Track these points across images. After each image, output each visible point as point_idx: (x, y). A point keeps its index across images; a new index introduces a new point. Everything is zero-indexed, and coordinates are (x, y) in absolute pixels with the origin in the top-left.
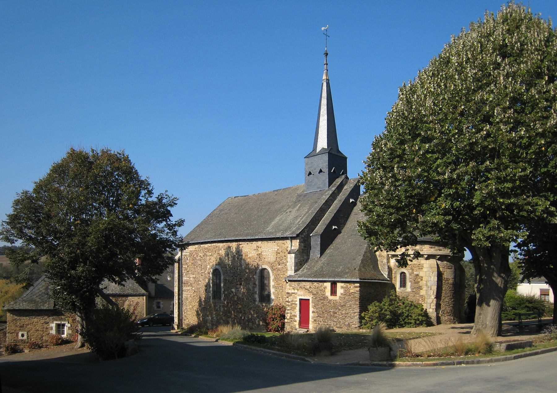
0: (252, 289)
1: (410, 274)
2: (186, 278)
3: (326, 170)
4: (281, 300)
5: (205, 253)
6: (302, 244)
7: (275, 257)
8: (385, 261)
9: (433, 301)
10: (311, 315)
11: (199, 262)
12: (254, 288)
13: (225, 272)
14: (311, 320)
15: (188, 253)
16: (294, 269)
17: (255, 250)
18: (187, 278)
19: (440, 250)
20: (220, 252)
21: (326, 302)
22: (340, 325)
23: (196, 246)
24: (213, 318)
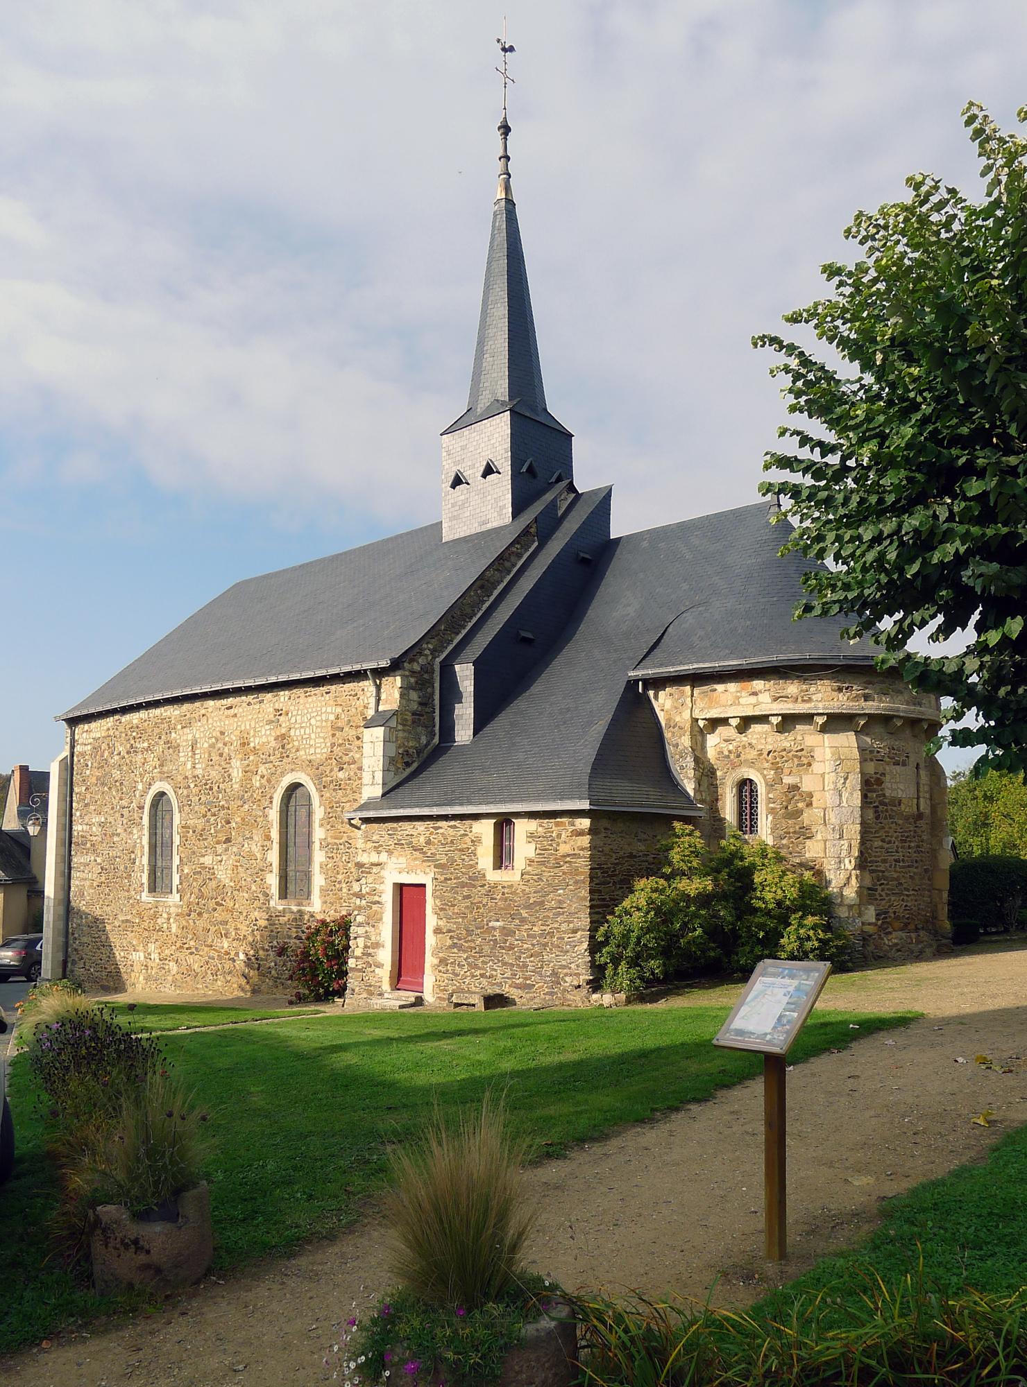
0: (259, 856)
1: (770, 786)
2: (80, 828)
3: (505, 466)
4: (344, 890)
5: (132, 742)
6: (414, 695)
7: (329, 744)
8: (686, 741)
9: (849, 878)
10: (430, 940)
11: (117, 774)
12: (265, 849)
13: (185, 803)
14: (430, 960)
15: (89, 747)
16: (381, 782)
18: (85, 827)
19: (867, 698)
20: (173, 735)
21: (478, 893)
22: (526, 979)
23: (110, 721)
24: (149, 954)
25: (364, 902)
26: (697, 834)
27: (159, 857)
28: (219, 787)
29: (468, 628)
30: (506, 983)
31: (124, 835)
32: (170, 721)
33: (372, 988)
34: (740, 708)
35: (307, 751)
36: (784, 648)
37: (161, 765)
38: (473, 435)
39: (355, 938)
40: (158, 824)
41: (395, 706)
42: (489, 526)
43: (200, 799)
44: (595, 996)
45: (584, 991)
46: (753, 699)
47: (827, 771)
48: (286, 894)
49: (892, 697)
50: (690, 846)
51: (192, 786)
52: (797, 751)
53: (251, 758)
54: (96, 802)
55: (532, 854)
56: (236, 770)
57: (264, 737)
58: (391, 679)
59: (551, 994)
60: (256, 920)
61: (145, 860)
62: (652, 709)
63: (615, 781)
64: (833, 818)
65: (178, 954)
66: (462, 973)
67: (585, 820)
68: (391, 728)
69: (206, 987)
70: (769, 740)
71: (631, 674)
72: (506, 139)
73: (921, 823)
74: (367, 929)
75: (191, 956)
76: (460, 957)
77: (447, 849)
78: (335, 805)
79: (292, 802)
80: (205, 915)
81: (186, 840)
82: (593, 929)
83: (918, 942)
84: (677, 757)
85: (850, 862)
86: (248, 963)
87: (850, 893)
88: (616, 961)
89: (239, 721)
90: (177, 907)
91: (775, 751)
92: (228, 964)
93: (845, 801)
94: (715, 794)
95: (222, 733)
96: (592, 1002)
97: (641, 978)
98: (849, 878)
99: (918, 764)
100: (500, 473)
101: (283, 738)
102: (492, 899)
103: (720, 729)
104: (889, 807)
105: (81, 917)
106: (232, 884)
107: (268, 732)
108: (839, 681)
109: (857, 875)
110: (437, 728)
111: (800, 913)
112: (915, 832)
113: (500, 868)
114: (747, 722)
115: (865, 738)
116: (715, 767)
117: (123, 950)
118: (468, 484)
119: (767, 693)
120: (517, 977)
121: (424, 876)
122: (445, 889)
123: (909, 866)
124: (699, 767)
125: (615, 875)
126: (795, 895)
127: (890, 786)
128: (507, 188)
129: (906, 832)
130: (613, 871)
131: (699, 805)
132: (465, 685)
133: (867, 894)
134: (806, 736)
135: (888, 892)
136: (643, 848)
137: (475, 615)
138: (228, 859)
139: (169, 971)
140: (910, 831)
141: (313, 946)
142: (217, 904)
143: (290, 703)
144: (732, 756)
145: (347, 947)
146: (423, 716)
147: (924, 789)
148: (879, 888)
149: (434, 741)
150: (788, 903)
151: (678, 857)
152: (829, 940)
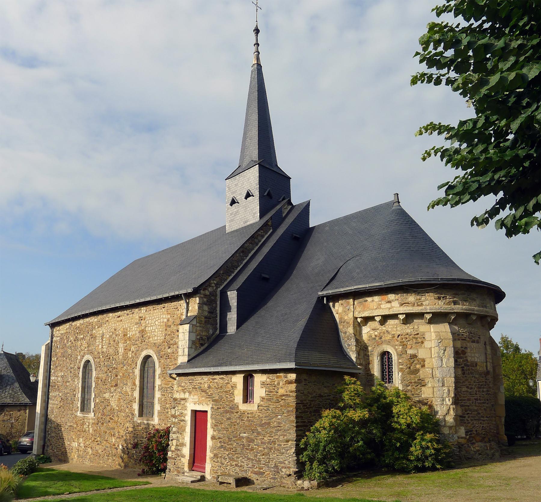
0: (130, 393)
1: (400, 355)
3: (256, 193)
5: (76, 335)
6: (206, 308)
8: (351, 330)
9: (449, 410)
10: (209, 443)
12: (133, 390)
14: (209, 454)
17: (137, 324)
19: (455, 303)
20: (94, 331)
22: (260, 469)
23: (67, 325)
24: (80, 444)
25: (176, 420)
26: (359, 383)
27: (86, 394)
28: (113, 358)
29: (235, 273)
30: (249, 470)
31: (71, 382)
32: (93, 324)
33: (179, 469)
34: (381, 310)
35: (154, 338)
36: (406, 275)
37: (88, 347)
38: (241, 178)
39: (172, 440)
40: (86, 377)
41: (195, 313)
42: (248, 223)
43: (104, 364)
44: (299, 482)
45: (293, 478)
46: (388, 305)
47: (433, 346)
48: (142, 414)
49: (470, 303)
50: (354, 390)
51: (101, 357)
52: (415, 335)
53: (128, 342)
54: (60, 365)
55: (263, 395)
56: (121, 348)
57: (134, 332)
58: (194, 299)
59: (274, 479)
60: (128, 428)
61: (80, 395)
62: (332, 313)
63: (310, 352)
64: (438, 374)
65: (92, 444)
66: (226, 463)
67: (293, 374)
68: (193, 325)
69: (104, 462)
70: (398, 329)
71: (320, 293)
72: (257, 35)
73: (489, 377)
74: (178, 435)
75: (98, 446)
76: (225, 453)
77: (219, 391)
78: (166, 367)
79: (146, 366)
80: (105, 424)
81: (98, 385)
82: (298, 440)
83: (491, 449)
84: (346, 339)
85: (449, 400)
86: (123, 451)
87: (450, 419)
88: (311, 460)
89: (123, 323)
90: (93, 419)
91: (402, 335)
92: (114, 451)
93: (444, 364)
94: (368, 360)
95: (115, 330)
96: (297, 485)
97: (327, 471)
98: (449, 410)
99: (485, 342)
100: (253, 196)
101: (143, 332)
102: (242, 420)
103: (370, 323)
104: (470, 368)
105: (52, 423)
106: (117, 408)
107: (136, 329)
108: (438, 293)
109: (453, 408)
110: (218, 326)
111: (422, 432)
112: (486, 382)
113: (246, 402)
114: (385, 318)
115: (454, 327)
116: (368, 345)
117: (68, 441)
118: (238, 203)
119: (397, 302)
120: (255, 467)
121: (207, 407)
122: (217, 414)
123: (483, 403)
124: (359, 345)
125: (311, 407)
126: (418, 421)
127: (470, 355)
128: (258, 59)
129: (480, 382)
130: (309, 405)
131: (359, 367)
132: (232, 302)
133: (460, 419)
134: (420, 326)
135: (472, 418)
136: (326, 391)
137: (239, 266)
138: (116, 395)
139: (88, 453)
140: (483, 382)
141: (151, 443)
142: (111, 418)
143: (146, 314)
144: (377, 338)
145: (168, 445)
146: (211, 319)
147: (489, 356)
148: (467, 416)
149: (216, 333)
150: (414, 425)
151: (348, 397)
152: (440, 449)
